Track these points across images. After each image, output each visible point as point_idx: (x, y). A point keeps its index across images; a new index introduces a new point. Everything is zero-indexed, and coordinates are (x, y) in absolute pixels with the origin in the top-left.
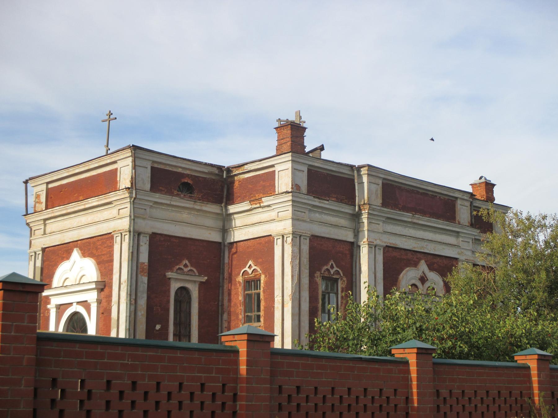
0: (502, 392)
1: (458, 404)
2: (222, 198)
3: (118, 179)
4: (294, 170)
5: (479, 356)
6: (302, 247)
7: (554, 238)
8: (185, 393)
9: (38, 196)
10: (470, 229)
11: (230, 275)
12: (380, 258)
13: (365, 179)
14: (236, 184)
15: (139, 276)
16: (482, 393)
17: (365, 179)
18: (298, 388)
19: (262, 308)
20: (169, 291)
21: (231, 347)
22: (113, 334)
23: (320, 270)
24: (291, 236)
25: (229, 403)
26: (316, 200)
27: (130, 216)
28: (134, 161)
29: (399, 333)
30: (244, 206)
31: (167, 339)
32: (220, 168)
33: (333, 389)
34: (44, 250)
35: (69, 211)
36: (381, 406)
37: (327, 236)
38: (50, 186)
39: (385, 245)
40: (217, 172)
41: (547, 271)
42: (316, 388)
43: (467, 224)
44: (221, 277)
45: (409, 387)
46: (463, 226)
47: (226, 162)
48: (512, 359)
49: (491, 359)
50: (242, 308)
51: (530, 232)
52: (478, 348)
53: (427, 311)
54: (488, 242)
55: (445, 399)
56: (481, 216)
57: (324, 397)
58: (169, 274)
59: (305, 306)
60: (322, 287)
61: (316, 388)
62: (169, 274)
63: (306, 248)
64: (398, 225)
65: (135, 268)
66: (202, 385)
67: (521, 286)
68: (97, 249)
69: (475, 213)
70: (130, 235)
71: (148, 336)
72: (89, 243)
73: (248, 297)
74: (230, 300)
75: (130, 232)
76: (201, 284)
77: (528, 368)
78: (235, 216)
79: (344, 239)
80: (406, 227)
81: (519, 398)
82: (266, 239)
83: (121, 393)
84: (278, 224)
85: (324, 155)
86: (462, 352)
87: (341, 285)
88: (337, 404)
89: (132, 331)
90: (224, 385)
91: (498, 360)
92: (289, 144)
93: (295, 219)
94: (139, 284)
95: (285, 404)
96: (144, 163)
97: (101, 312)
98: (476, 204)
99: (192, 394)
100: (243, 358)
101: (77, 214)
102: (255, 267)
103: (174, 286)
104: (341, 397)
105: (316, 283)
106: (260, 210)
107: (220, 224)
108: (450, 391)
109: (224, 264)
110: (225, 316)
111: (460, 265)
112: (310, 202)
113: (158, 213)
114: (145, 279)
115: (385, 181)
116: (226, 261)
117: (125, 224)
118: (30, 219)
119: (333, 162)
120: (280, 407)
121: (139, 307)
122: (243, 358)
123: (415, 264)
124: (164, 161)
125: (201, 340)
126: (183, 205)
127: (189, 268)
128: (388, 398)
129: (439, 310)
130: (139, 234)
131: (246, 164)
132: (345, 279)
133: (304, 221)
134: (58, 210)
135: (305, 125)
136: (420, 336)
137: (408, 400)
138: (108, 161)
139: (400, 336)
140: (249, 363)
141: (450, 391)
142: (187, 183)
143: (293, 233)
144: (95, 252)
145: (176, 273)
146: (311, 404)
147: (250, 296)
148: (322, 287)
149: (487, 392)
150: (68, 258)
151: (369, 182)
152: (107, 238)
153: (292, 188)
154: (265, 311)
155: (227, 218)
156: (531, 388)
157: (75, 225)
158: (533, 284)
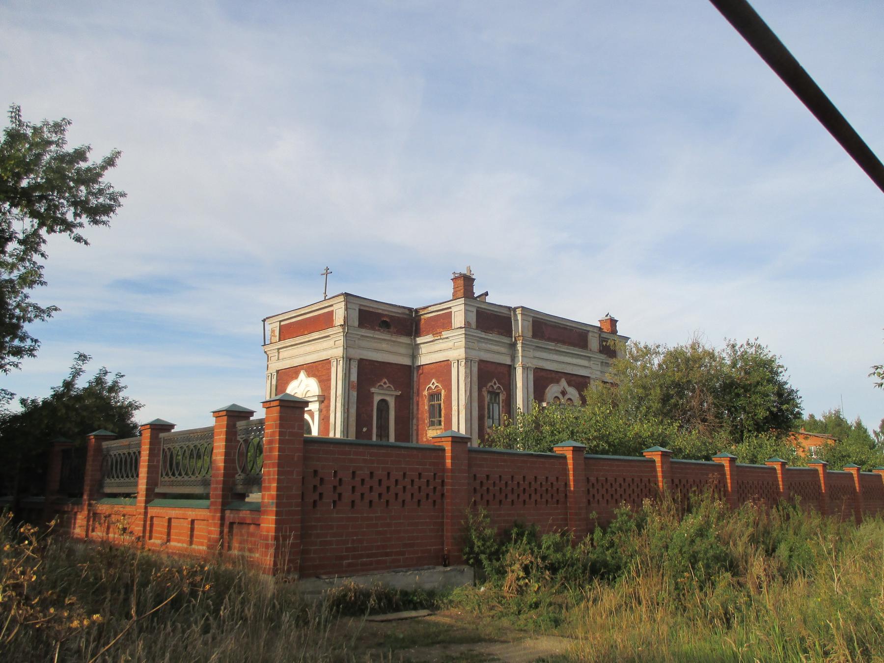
0: (635, 479)
1: (603, 488)
2: (412, 332)
3: (334, 318)
4: (466, 311)
5: (615, 453)
6: (472, 369)
7: (665, 362)
8: (408, 480)
9: (273, 331)
10: (599, 354)
11: (418, 390)
12: (531, 377)
13: (519, 317)
14: (423, 321)
15: (351, 391)
16: (620, 480)
17: (519, 317)
18: (488, 476)
19: (443, 415)
20: (372, 402)
21: (440, 446)
22: (331, 435)
23: (485, 386)
24: (464, 360)
25: (439, 488)
26: (483, 333)
27: (343, 346)
28: (346, 305)
29: (556, 435)
30: (429, 338)
31: (371, 439)
32: (410, 309)
33: (512, 477)
34: (278, 372)
35: (297, 342)
36: (547, 490)
37: (492, 360)
38: (282, 323)
39: (535, 367)
40: (407, 312)
41: (661, 386)
42: (500, 476)
43: (597, 351)
44: (412, 391)
45: (567, 475)
46: (593, 352)
47: (414, 306)
48: (641, 455)
49: (624, 454)
50: (427, 415)
51: (647, 357)
52: (614, 446)
53: (576, 418)
54: (615, 365)
55: (593, 484)
56: (609, 346)
57: (506, 483)
58: (373, 390)
59: (475, 414)
60: (487, 398)
61: (500, 476)
62: (373, 390)
63: (475, 369)
64: (545, 352)
65: (347, 385)
66: (420, 474)
67: (641, 399)
68: (318, 371)
69: (604, 343)
70: (343, 360)
71: (357, 437)
72: (313, 366)
73: (432, 407)
74: (418, 409)
75: (343, 358)
76: (397, 397)
77: (654, 461)
78: (422, 346)
79: (504, 362)
80: (550, 353)
81: (648, 484)
82: (446, 363)
83: (363, 480)
84: (454, 351)
85: (489, 299)
86: (604, 449)
87: (502, 397)
88: (516, 488)
89: (346, 433)
90: (435, 474)
91: (629, 455)
92: (462, 291)
93: (467, 348)
94: (351, 397)
95: (478, 488)
96: (353, 306)
97: (322, 418)
98: (604, 335)
99: (412, 481)
100: (448, 454)
101: (303, 345)
102: (437, 384)
103: (377, 399)
104: (518, 483)
105: (483, 396)
106: (441, 341)
107: (410, 352)
108: (597, 478)
109: (413, 381)
110: (415, 421)
111: (592, 382)
112: (478, 335)
113: (364, 343)
114: (355, 394)
115: (534, 319)
116: (415, 379)
117: (339, 352)
118: (267, 348)
119: (495, 305)
120: (475, 490)
121: (350, 415)
122: (448, 454)
123: (558, 381)
124: (368, 305)
125: (397, 439)
126: (383, 337)
127: (388, 385)
128: (552, 484)
129: (586, 418)
130: (350, 360)
131: (430, 306)
132: (504, 393)
133: (475, 349)
134: (288, 342)
135: (473, 277)
136: (572, 437)
137: (566, 485)
138: (327, 305)
139: (557, 437)
140: (453, 458)
141: (597, 478)
142: (385, 321)
143: (466, 359)
144: (317, 373)
145: (378, 388)
146: (497, 488)
147: (433, 406)
148: (487, 398)
149: (624, 479)
150: (296, 378)
151: (522, 320)
152: (327, 362)
153: (465, 324)
154: (445, 417)
155: (416, 347)
156: (656, 476)
157: (302, 353)
158: (650, 397)
